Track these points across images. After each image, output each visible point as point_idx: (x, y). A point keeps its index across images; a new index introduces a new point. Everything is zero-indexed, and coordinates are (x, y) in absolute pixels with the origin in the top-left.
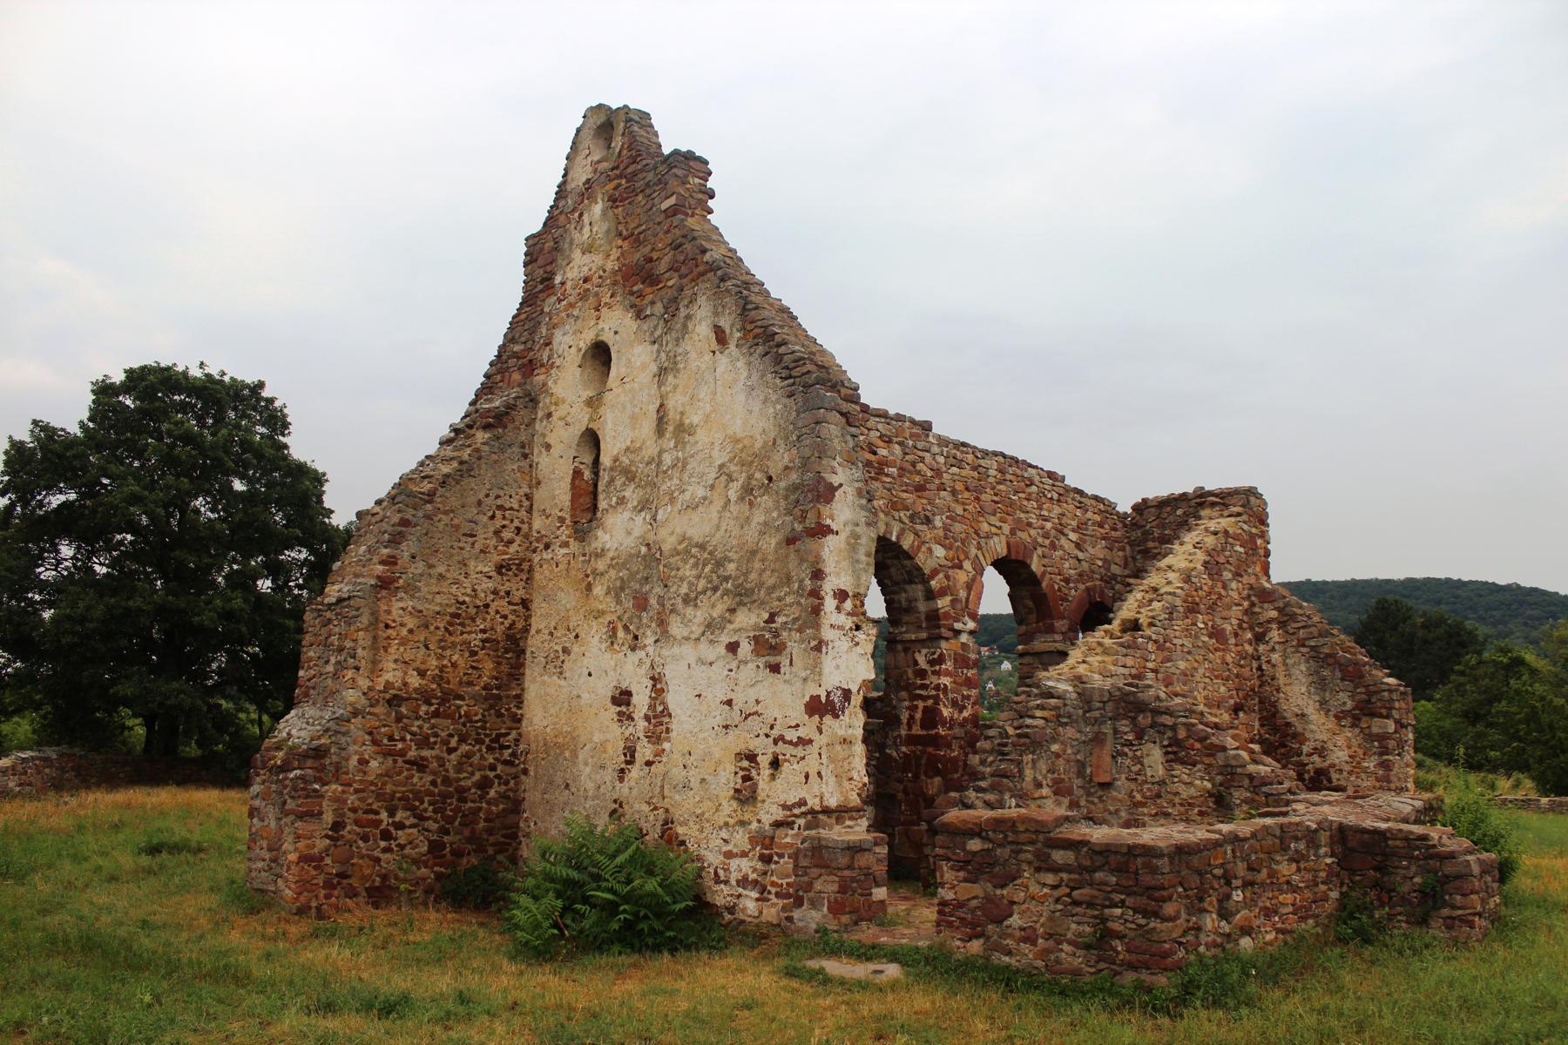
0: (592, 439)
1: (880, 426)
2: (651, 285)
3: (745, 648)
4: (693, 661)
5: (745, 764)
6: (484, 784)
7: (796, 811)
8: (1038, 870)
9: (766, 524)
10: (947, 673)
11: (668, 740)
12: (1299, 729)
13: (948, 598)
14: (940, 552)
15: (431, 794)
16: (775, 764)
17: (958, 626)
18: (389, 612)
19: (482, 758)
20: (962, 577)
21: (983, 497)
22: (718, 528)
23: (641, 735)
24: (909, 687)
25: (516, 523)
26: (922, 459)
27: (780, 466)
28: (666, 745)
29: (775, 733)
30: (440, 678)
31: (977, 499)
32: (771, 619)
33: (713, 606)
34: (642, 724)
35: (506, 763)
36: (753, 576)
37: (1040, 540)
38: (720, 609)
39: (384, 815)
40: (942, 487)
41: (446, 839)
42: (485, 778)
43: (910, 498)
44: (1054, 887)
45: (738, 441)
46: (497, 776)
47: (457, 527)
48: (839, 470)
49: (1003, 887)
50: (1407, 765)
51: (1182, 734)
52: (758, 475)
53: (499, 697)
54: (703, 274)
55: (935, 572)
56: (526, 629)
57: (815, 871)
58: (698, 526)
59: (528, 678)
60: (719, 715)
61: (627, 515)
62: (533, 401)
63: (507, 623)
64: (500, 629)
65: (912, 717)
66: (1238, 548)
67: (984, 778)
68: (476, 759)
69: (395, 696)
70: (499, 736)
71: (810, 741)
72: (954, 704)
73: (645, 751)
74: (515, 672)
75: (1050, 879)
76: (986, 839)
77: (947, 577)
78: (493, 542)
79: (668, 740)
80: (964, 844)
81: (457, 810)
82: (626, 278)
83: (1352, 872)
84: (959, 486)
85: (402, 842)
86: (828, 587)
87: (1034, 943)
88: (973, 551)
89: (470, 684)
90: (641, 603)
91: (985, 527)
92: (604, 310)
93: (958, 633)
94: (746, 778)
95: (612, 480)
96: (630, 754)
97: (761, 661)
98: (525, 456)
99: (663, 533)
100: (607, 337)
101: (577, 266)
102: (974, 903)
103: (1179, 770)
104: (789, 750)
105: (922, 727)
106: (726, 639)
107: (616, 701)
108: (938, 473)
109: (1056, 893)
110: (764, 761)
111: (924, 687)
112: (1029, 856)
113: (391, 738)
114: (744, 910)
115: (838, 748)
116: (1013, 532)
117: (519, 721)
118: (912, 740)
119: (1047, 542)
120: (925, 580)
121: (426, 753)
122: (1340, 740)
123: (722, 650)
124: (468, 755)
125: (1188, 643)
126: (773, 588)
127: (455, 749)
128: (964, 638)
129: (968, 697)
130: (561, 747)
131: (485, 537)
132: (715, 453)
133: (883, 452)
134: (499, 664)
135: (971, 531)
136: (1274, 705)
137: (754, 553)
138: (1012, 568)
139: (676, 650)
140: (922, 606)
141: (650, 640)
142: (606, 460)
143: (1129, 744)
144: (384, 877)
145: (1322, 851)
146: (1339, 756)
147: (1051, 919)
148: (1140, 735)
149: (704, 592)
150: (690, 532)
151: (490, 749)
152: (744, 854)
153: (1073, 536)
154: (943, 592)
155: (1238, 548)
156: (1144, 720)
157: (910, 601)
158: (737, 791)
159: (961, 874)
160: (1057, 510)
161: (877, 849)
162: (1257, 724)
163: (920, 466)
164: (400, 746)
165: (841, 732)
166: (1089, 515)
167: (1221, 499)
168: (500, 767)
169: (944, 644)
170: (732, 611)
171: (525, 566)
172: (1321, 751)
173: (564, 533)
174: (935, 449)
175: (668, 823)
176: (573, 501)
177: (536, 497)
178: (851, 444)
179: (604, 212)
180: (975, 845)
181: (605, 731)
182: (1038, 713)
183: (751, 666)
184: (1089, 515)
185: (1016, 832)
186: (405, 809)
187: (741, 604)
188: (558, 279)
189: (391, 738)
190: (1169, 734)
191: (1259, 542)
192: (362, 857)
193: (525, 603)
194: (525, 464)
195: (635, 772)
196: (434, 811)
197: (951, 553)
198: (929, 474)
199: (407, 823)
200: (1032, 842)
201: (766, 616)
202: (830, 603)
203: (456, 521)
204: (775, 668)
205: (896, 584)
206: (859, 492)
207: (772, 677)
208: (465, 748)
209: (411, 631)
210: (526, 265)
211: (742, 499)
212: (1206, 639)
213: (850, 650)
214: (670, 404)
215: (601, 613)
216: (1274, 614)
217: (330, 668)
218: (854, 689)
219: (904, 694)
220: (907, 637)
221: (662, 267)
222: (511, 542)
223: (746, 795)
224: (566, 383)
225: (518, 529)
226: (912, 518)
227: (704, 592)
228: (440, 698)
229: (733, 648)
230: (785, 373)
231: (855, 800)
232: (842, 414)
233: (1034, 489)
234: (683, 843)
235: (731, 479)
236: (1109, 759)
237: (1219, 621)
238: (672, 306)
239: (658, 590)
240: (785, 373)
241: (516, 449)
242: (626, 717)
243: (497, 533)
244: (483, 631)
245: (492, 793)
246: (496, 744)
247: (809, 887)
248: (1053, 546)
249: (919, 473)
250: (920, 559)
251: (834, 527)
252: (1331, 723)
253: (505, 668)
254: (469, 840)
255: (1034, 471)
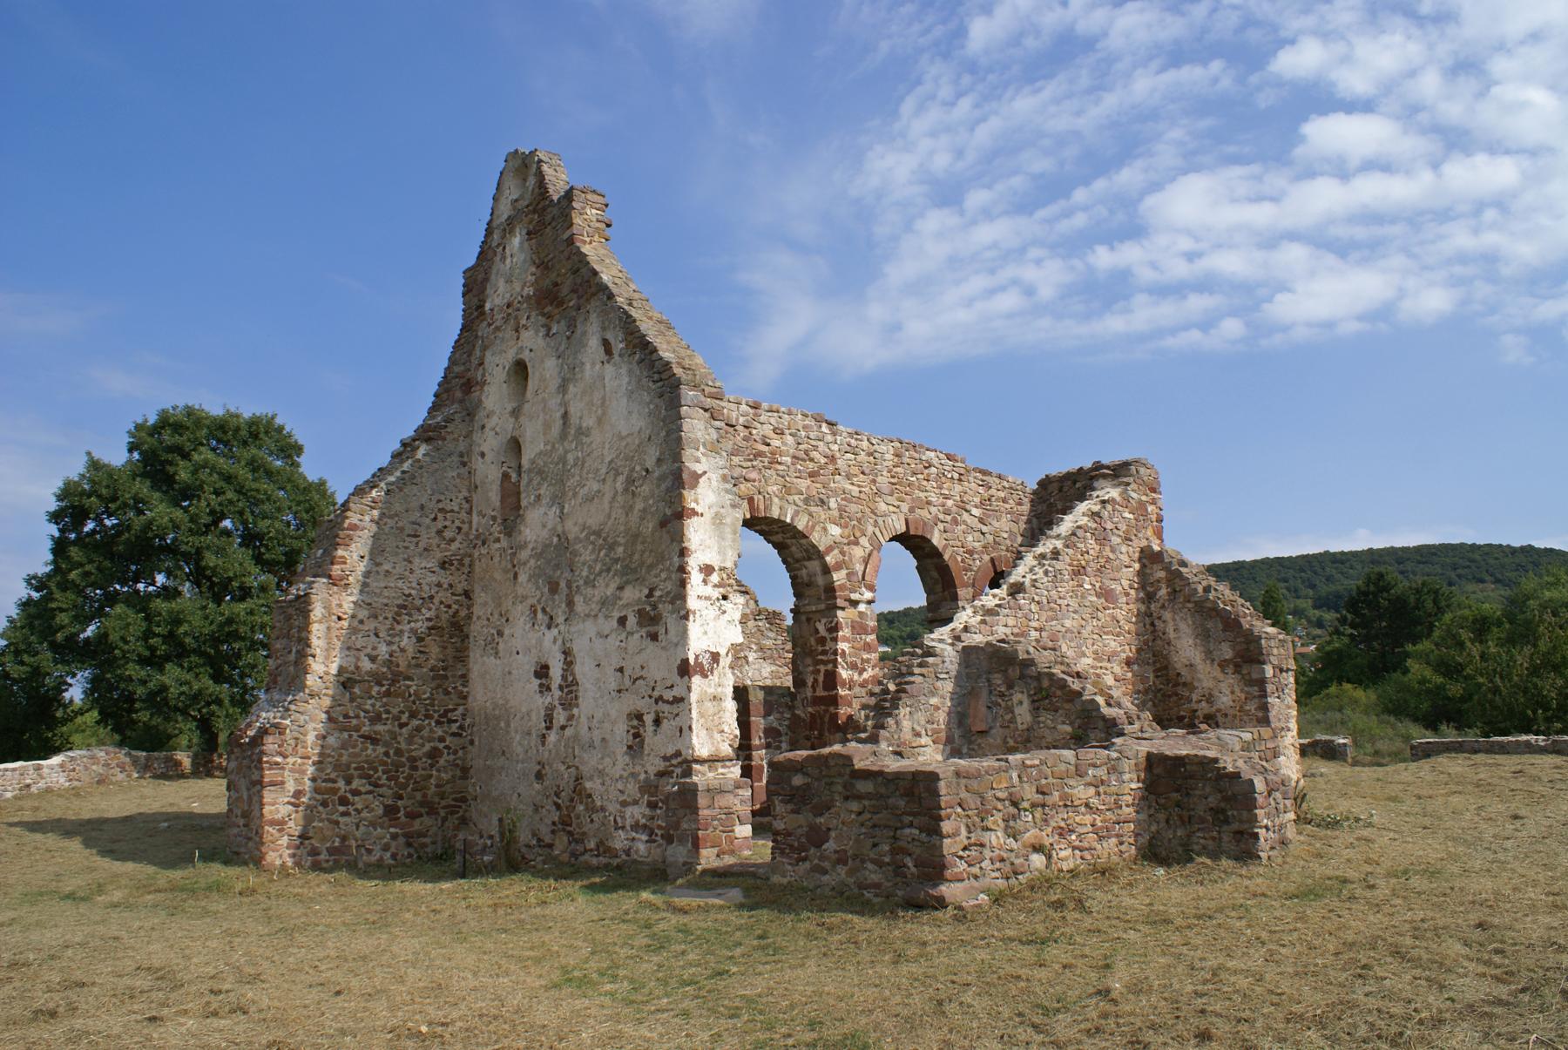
0: (515, 446)
1: (772, 421)
2: (558, 306)
3: (632, 621)
4: (593, 635)
5: (635, 722)
6: (434, 754)
7: (674, 762)
8: (847, 798)
9: (644, 510)
10: (846, 639)
11: (577, 706)
12: (1189, 679)
13: (844, 572)
14: (835, 531)
15: (385, 764)
16: (657, 722)
17: (854, 596)
18: (340, 606)
19: (431, 731)
20: (858, 552)
21: (879, 479)
22: (609, 516)
23: (556, 703)
24: (812, 653)
25: (457, 523)
26: (815, 448)
27: (654, 459)
28: (575, 711)
29: (656, 694)
30: (389, 663)
31: (874, 481)
32: (650, 595)
33: (607, 585)
34: (557, 693)
35: (454, 734)
36: (636, 557)
37: (941, 516)
38: (613, 586)
39: (341, 784)
40: (837, 472)
41: (400, 803)
42: (435, 749)
43: (803, 484)
44: (859, 814)
45: (622, 438)
46: (447, 747)
47: (402, 529)
48: (703, 459)
49: (821, 815)
50: (1289, 707)
51: (1045, 683)
52: (638, 468)
53: (446, 677)
54: (594, 295)
55: (830, 549)
56: (469, 617)
57: (681, 812)
58: (594, 516)
59: (472, 659)
60: (612, 682)
61: (542, 510)
62: (470, 415)
63: (451, 612)
64: (444, 617)
65: (816, 680)
66: (1127, 515)
67: (865, 731)
68: (425, 733)
69: (349, 679)
70: (446, 712)
71: (682, 700)
72: (853, 666)
73: (560, 717)
74: (461, 656)
75: (855, 806)
76: (806, 774)
77: (843, 553)
78: (436, 541)
79: (577, 706)
80: (790, 779)
81: (410, 777)
82: (538, 303)
83: (1158, 795)
84: (854, 470)
85: (359, 807)
86: (694, 563)
87: (845, 863)
88: (870, 529)
89: (418, 666)
90: (554, 589)
91: (882, 507)
92: (522, 331)
93: (855, 603)
94: (636, 735)
95: (531, 480)
96: (549, 719)
97: (643, 632)
98: (464, 464)
99: (569, 524)
100: (526, 356)
101: (499, 294)
102: (799, 831)
103: (1046, 718)
104: (666, 708)
105: (825, 688)
106: (616, 615)
107: (538, 675)
108: (832, 459)
109: (861, 818)
110: (648, 719)
111: (824, 653)
112: (840, 788)
113: (346, 716)
114: (637, 851)
115: (709, 704)
116: (911, 510)
117: (465, 698)
118: (817, 701)
119: (949, 518)
120: (820, 556)
121: (379, 727)
122: (1224, 687)
123: (615, 623)
124: (418, 729)
125: (1074, 603)
126: (651, 567)
127: (406, 724)
128: (862, 607)
129: (868, 661)
130: (498, 718)
131: (428, 537)
132: (606, 452)
133: (776, 443)
134: (445, 648)
135: (867, 510)
136: (1166, 658)
137: (636, 536)
138: (913, 542)
139: (581, 626)
140: (820, 580)
141: (560, 620)
142: (525, 462)
143: (1002, 695)
144: (344, 839)
145: (1126, 777)
146: (1225, 700)
147: (857, 841)
148: (1010, 686)
149: (600, 574)
150: (590, 522)
151: (438, 723)
152: (636, 802)
153: (975, 511)
154: (838, 567)
155: (1127, 515)
156: (1014, 672)
157: (809, 575)
158: (630, 747)
159: (790, 807)
160: (958, 488)
161: (740, 792)
162: (1151, 676)
163: (814, 454)
164: (354, 722)
165: (711, 691)
166: (993, 491)
167: (1119, 472)
168: (448, 739)
169: (840, 613)
170: (621, 588)
171: (467, 561)
172: (1209, 698)
173: (496, 528)
174: (829, 438)
175: (578, 778)
176: (502, 501)
177: (475, 498)
178: (715, 436)
179: (521, 243)
180: (798, 780)
181: (527, 699)
182: (917, 670)
183: (637, 636)
184: (993, 491)
185: (828, 767)
186: (360, 777)
187: (628, 582)
188: (488, 306)
189: (346, 716)
190: (1035, 684)
191: (1150, 508)
192: (321, 820)
193: (467, 594)
194: (463, 471)
195: (552, 737)
196: (389, 779)
197: (846, 531)
198: (823, 460)
199: (363, 789)
200: (840, 775)
201: (646, 591)
202: (695, 578)
203: (400, 524)
204: (654, 637)
205: (798, 561)
206: (724, 478)
207: (651, 646)
208: (416, 722)
209: (361, 622)
210: (464, 295)
211: (626, 490)
212: (1094, 599)
213: (717, 618)
214: (572, 410)
215: (525, 598)
216: (1162, 574)
217: (292, 657)
218: (723, 652)
219: (809, 661)
220: (808, 608)
221: (565, 290)
222: (452, 540)
223: (636, 745)
224: (495, 396)
225: (459, 529)
226: (806, 501)
227: (600, 574)
228: (391, 678)
229: (622, 621)
230: (656, 377)
231: (726, 750)
232: (706, 410)
233: (933, 470)
234: (590, 796)
235: (617, 474)
236: (984, 709)
237: (1107, 583)
238: (572, 326)
239: (567, 575)
240: (656, 377)
241: (455, 459)
242: (545, 688)
243: (439, 532)
244: (429, 620)
245: (442, 762)
246: (445, 718)
247: (677, 826)
248: (955, 522)
249: (812, 460)
250: (816, 538)
251: (699, 509)
252: (1217, 672)
253: (450, 651)
254: (422, 804)
255: (932, 454)
